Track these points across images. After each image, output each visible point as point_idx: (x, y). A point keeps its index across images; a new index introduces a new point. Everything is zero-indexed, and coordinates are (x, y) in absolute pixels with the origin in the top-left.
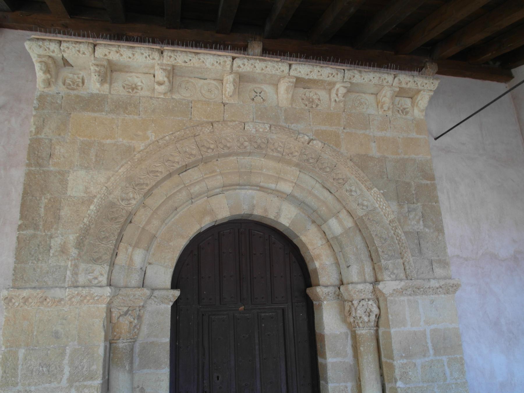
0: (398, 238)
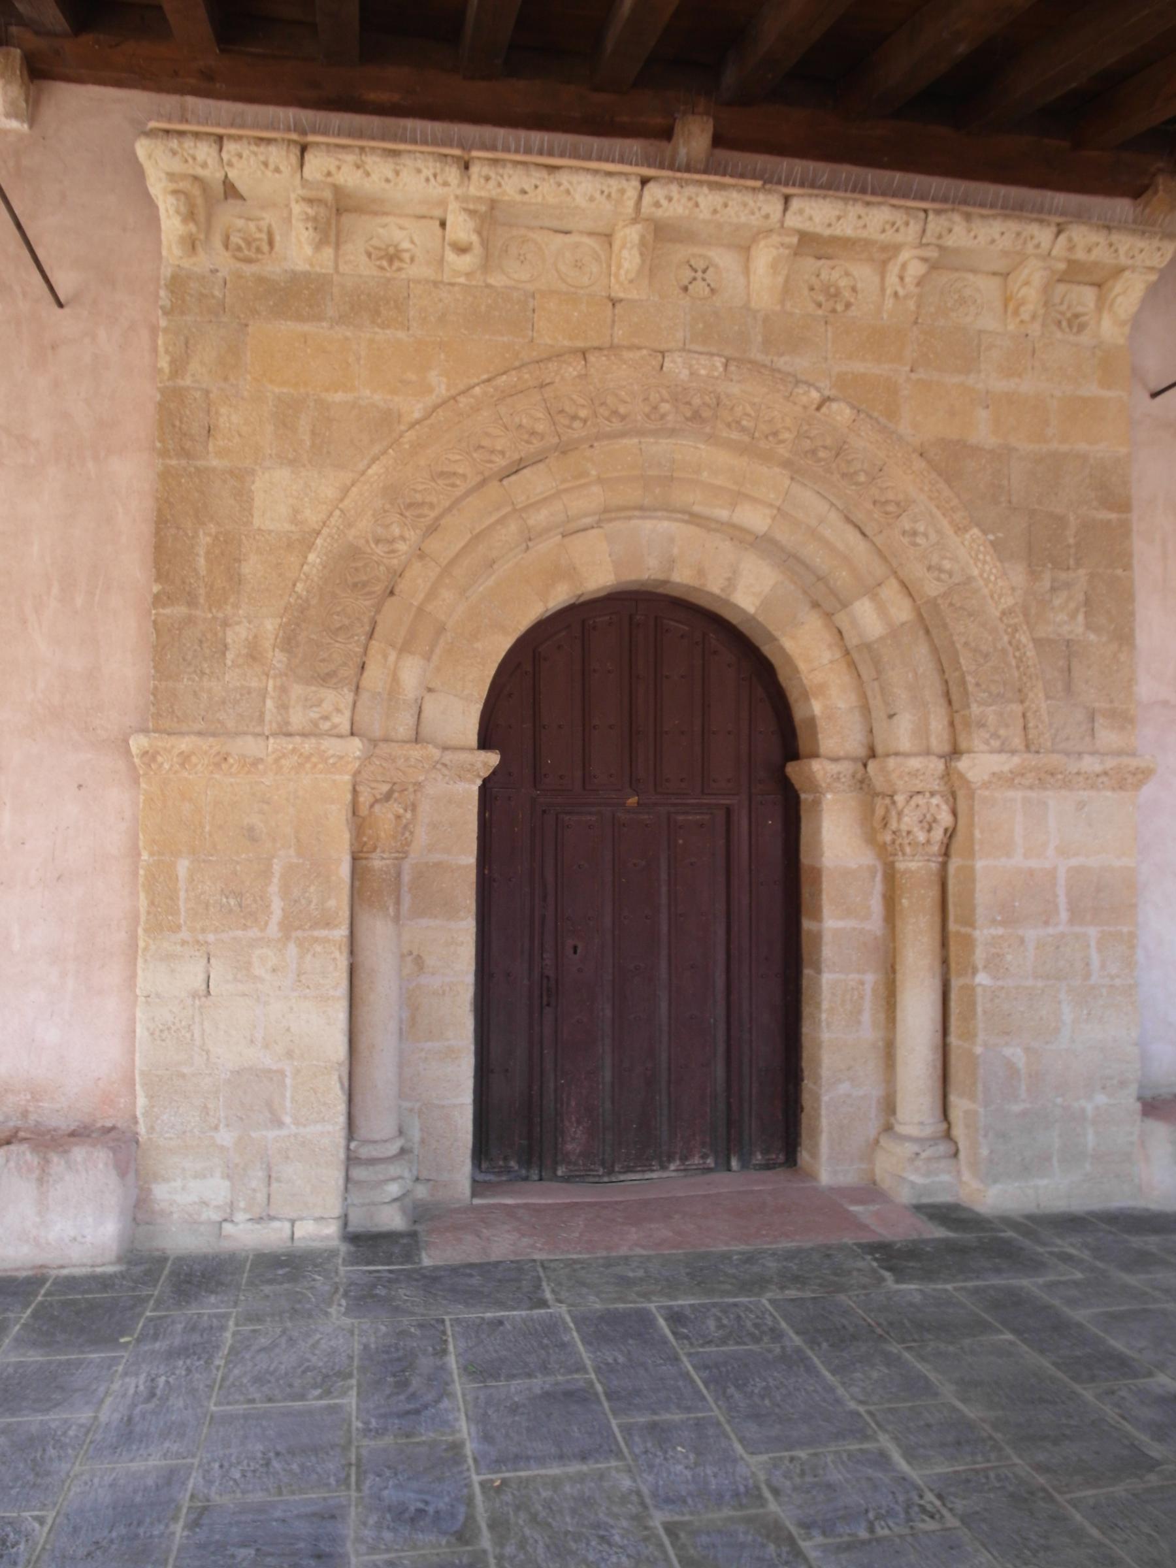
0: (1017, 654)
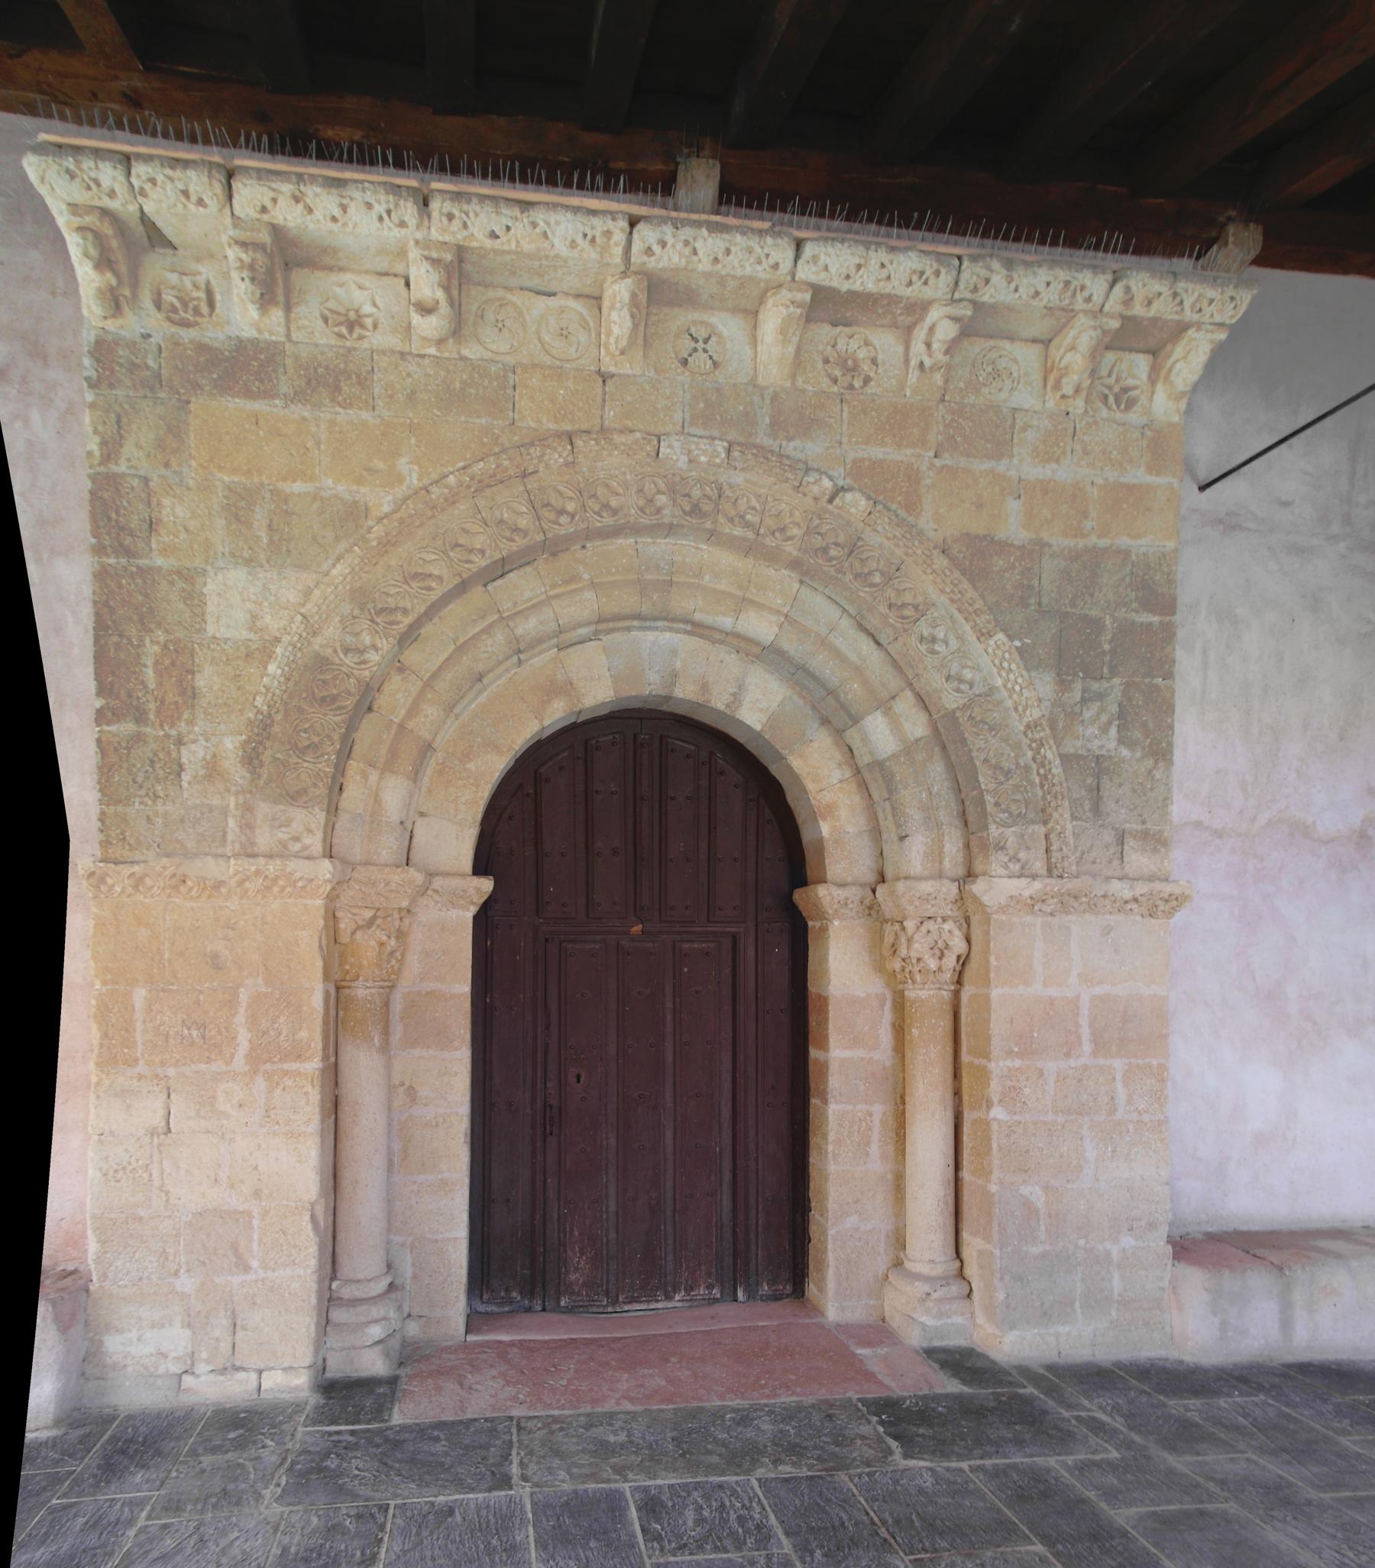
0: (1042, 771)
